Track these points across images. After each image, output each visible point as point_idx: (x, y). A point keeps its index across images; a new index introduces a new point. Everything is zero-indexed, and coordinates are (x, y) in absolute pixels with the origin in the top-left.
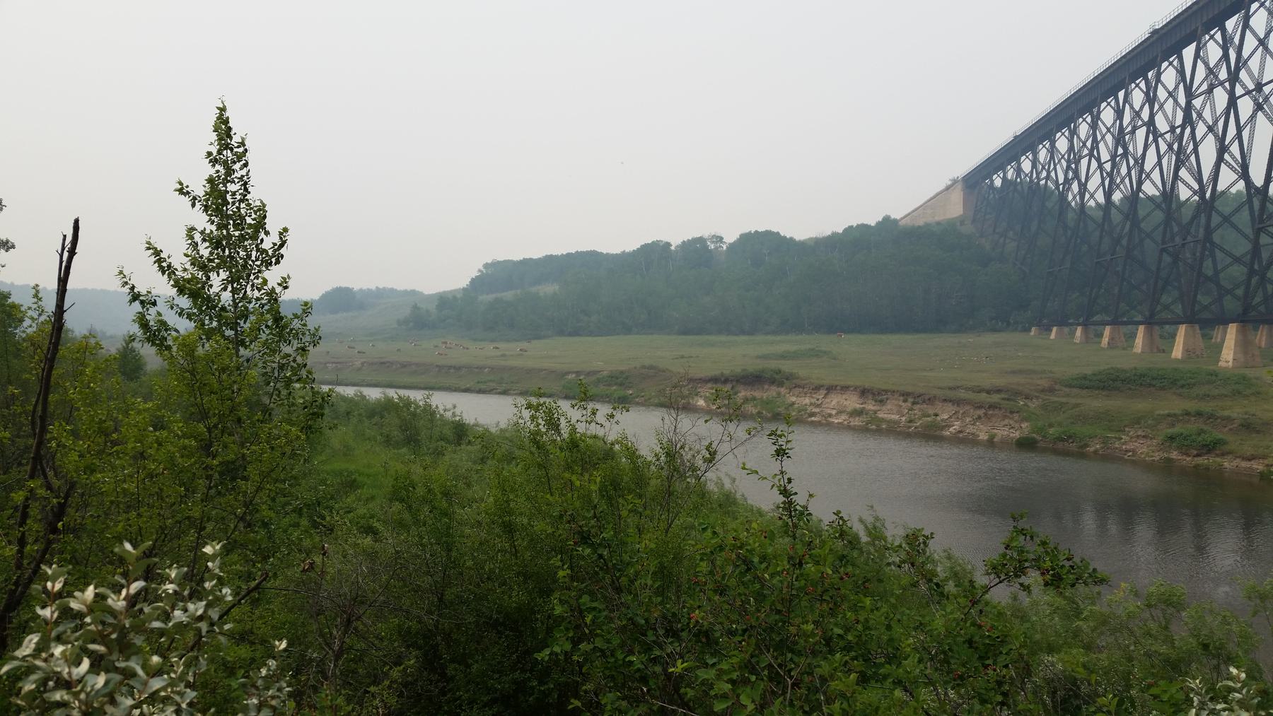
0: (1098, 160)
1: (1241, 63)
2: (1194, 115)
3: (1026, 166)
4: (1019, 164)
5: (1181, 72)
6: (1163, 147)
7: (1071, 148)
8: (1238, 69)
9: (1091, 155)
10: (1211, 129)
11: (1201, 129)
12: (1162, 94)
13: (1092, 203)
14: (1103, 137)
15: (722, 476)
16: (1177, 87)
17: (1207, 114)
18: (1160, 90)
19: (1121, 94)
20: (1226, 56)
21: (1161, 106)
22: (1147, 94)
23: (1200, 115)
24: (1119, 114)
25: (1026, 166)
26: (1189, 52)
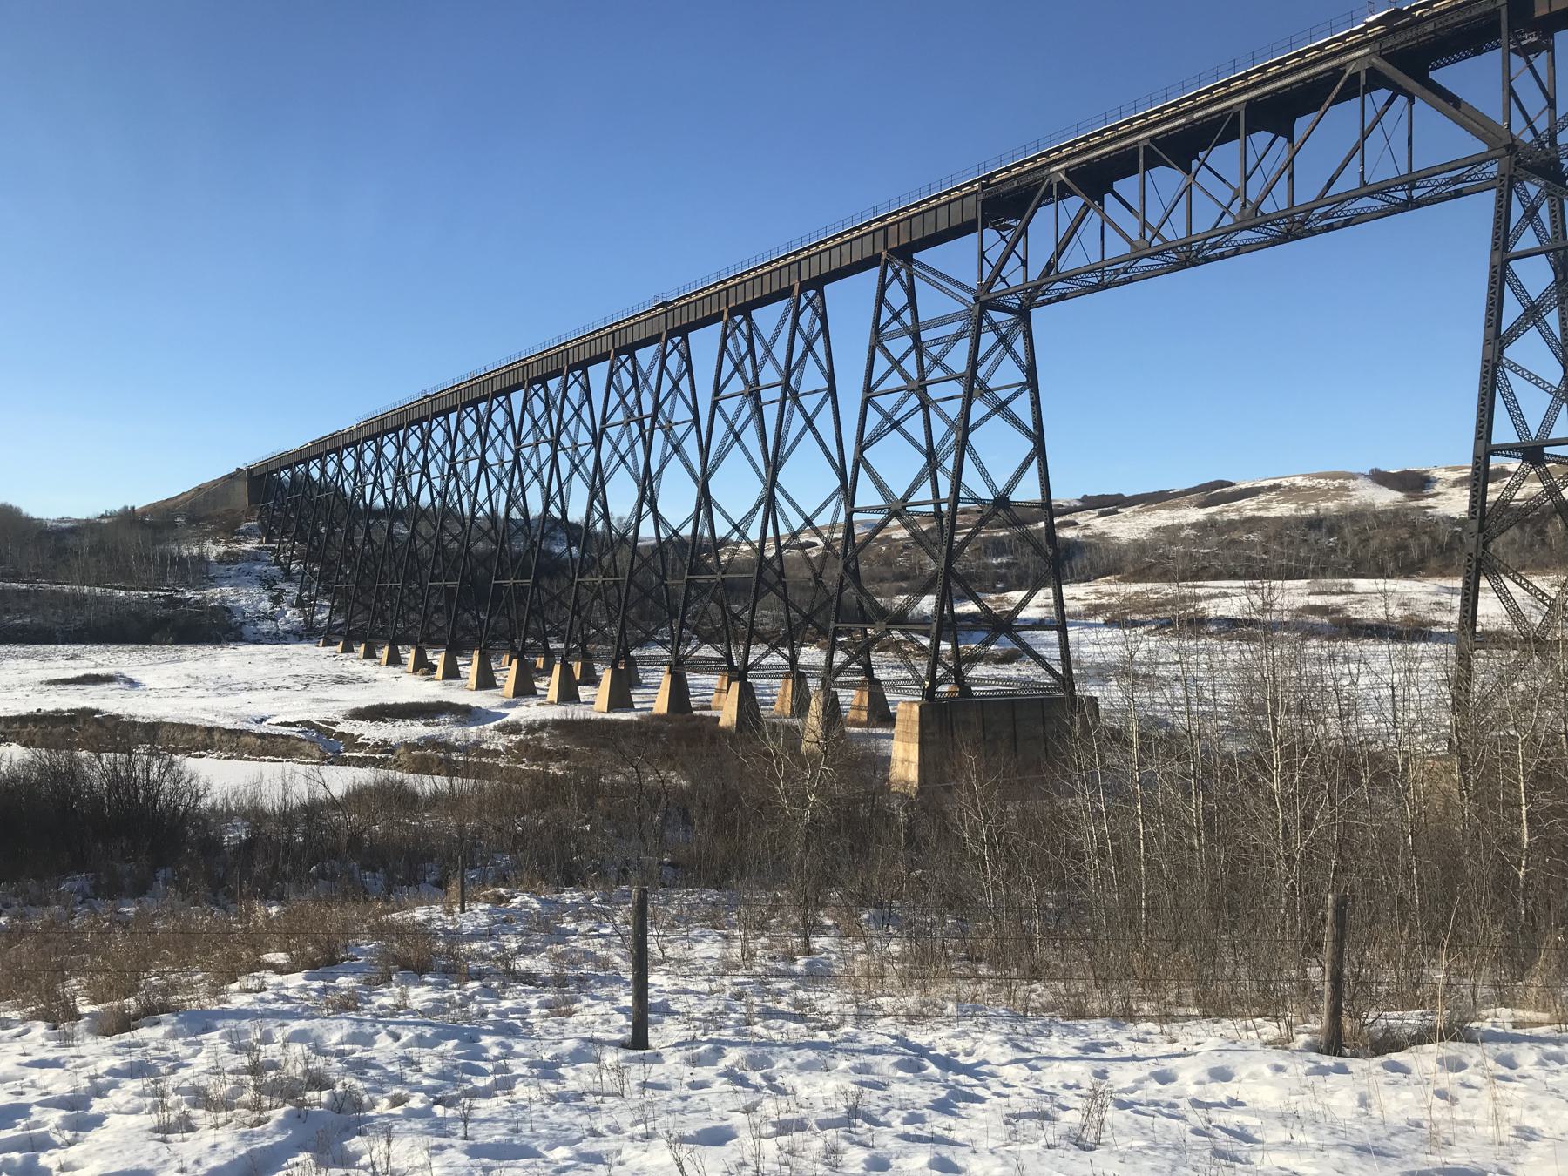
0: (428, 476)
1: (562, 426)
2: (523, 464)
3: (331, 468)
4: (341, 460)
5: (510, 414)
6: (493, 483)
7: (357, 468)
8: (559, 433)
9: (374, 484)
10: (536, 476)
11: (528, 476)
12: (493, 432)
13: (480, 514)
14: (434, 457)
15: (453, 1141)
16: (505, 428)
17: (534, 464)
18: (492, 429)
19: (453, 417)
20: (479, 431)
21: (492, 443)
22: (422, 441)
23: (528, 464)
24: (399, 450)
25: (331, 468)
26: (517, 397)
